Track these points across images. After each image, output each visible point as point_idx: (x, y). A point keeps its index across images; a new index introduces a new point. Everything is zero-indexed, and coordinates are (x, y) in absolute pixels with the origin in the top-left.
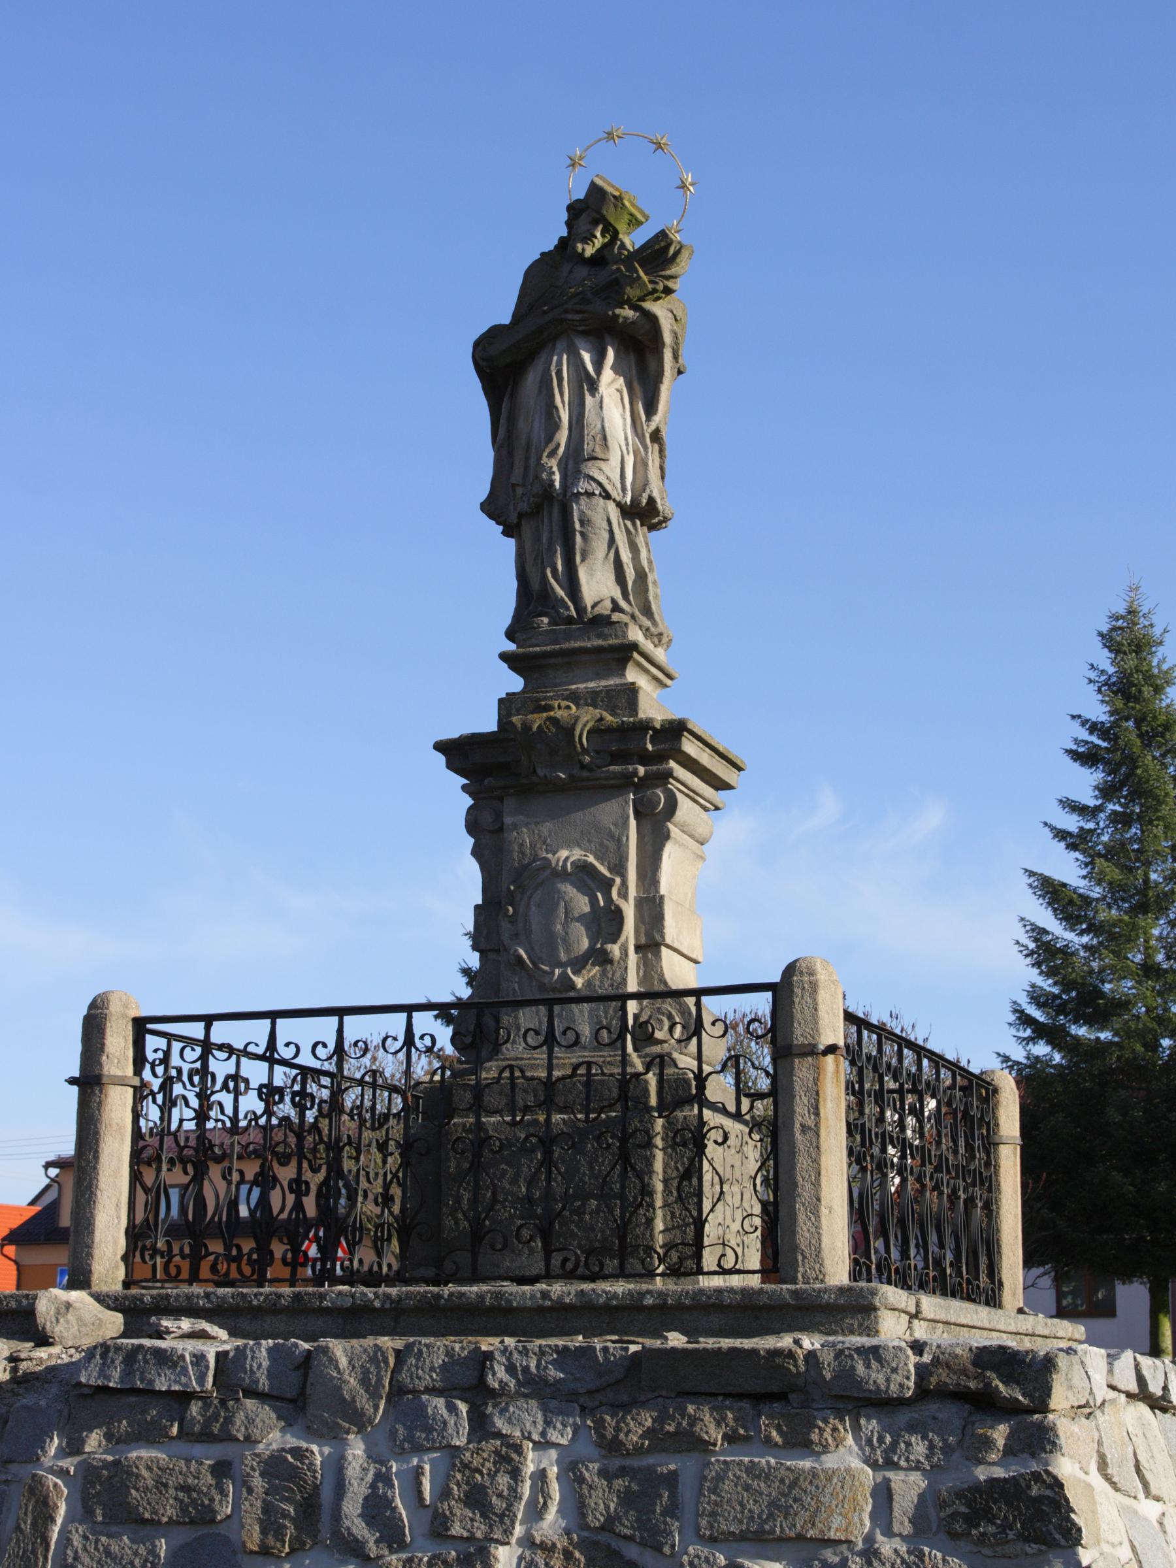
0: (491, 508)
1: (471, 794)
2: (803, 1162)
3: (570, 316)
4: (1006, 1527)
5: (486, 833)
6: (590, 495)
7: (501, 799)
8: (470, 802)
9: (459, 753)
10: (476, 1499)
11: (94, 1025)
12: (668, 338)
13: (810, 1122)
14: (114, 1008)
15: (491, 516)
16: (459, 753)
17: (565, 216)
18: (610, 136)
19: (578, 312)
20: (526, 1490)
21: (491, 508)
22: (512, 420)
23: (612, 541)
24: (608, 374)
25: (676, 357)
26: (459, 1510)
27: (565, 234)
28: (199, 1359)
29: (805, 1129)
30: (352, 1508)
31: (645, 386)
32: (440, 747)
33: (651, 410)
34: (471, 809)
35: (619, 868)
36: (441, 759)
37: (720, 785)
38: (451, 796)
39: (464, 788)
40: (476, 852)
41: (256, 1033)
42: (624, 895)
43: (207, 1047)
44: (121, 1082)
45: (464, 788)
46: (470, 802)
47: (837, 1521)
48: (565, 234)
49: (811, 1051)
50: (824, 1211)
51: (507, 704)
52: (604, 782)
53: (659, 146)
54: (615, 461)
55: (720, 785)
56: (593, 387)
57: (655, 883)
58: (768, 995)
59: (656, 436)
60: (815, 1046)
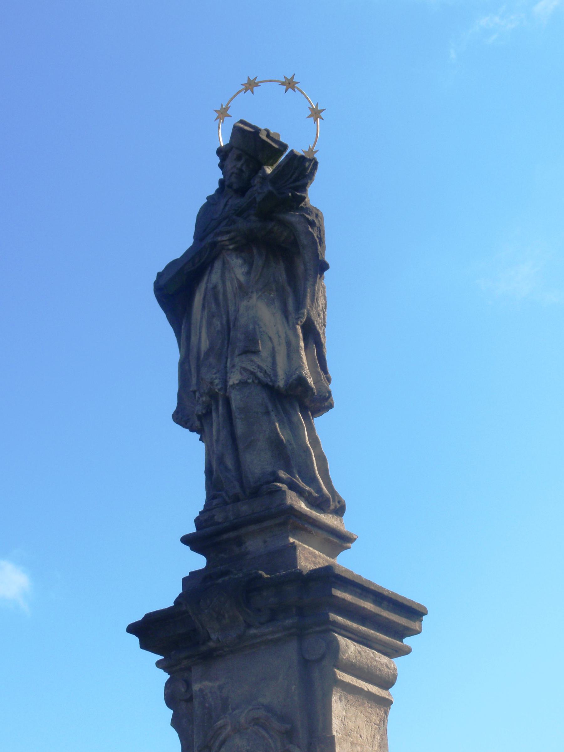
0: (182, 417)
1: (166, 669)
3: (219, 239)
7: (189, 669)
8: (166, 676)
9: (150, 631)
15: (185, 425)
16: (150, 631)
17: (218, 160)
19: (228, 232)
21: (182, 417)
22: (188, 338)
27: (222, 177)
34: (168, 684)
36: (134, 640)
38: (148, 674)
39: (159, 664)
40: (176, 723)
45: (159, 664)
46: (166, 676)
48: (222, 177)
52: (270, 637)
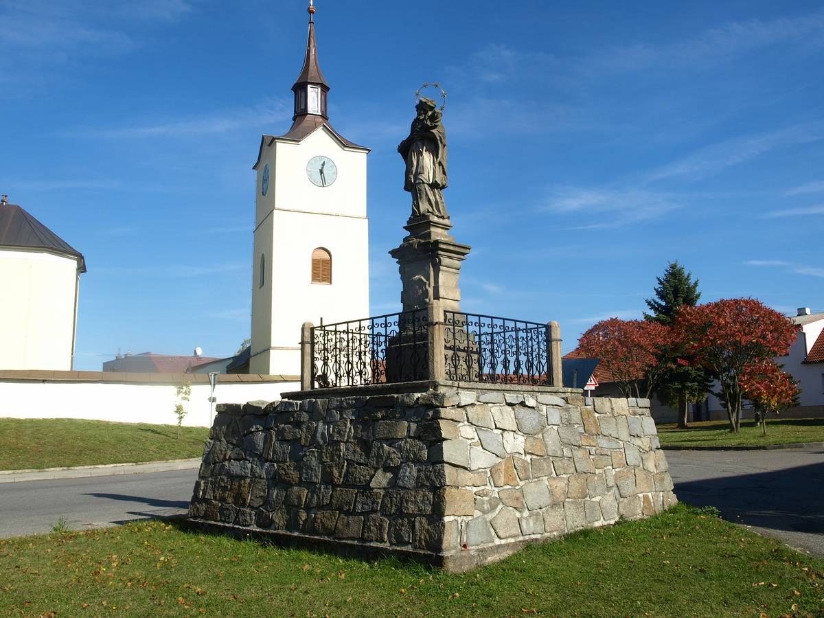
2: (430, 351)
4: (429, 434)
5: (405, 275)
6: (419, 183)
9: (394, 253)
10: (339, 432)
11: (303, 329)
12: (438, 138)
13: (432, 341)
14: (306, 326)
16: (394, 253)
18: (425, 86)
20: (348, 430)
23: (427, 195)
24: (424, 152)
25: (442, 143)
26: (337, 435)
28: (297, 404)
29: (431, 343)
30: (319, 435)
31: (435, 152)
32: (389, 253)
33: (437, 158)
35: (428, 279)
37: (463, 254)
41: (475, 319)
42: (429, 286)
43: (336, 332)
44: (308, 343)
47: (400, 434)
49: (433, 324)
50: (435, 363)
51: (406, 240)
53: (436, 86)
54: (426, 173)
55: (463, 254)
56: (422, 155)
57: (438, 283)
58: (398, 316)
59: (440, 164)
60: (433, 322)
